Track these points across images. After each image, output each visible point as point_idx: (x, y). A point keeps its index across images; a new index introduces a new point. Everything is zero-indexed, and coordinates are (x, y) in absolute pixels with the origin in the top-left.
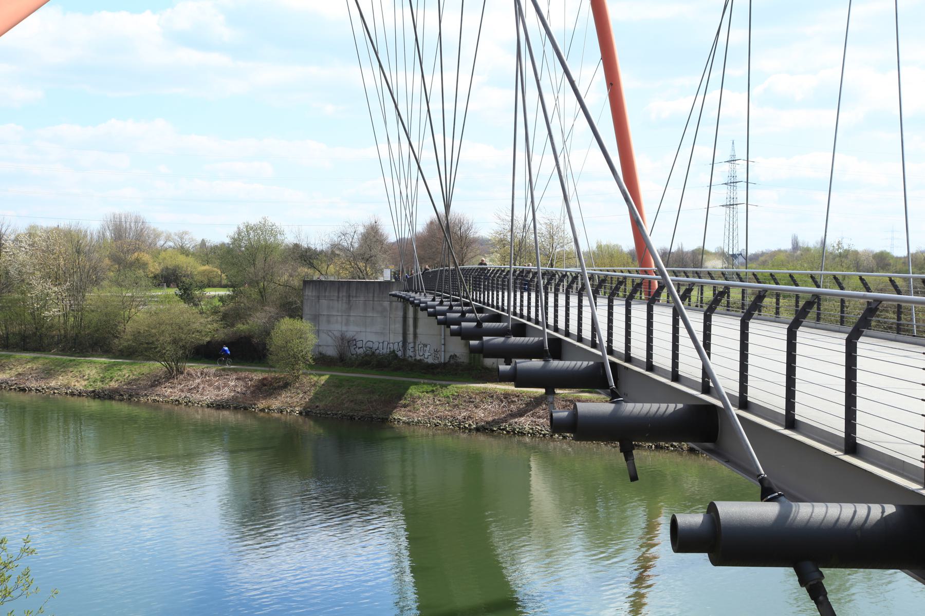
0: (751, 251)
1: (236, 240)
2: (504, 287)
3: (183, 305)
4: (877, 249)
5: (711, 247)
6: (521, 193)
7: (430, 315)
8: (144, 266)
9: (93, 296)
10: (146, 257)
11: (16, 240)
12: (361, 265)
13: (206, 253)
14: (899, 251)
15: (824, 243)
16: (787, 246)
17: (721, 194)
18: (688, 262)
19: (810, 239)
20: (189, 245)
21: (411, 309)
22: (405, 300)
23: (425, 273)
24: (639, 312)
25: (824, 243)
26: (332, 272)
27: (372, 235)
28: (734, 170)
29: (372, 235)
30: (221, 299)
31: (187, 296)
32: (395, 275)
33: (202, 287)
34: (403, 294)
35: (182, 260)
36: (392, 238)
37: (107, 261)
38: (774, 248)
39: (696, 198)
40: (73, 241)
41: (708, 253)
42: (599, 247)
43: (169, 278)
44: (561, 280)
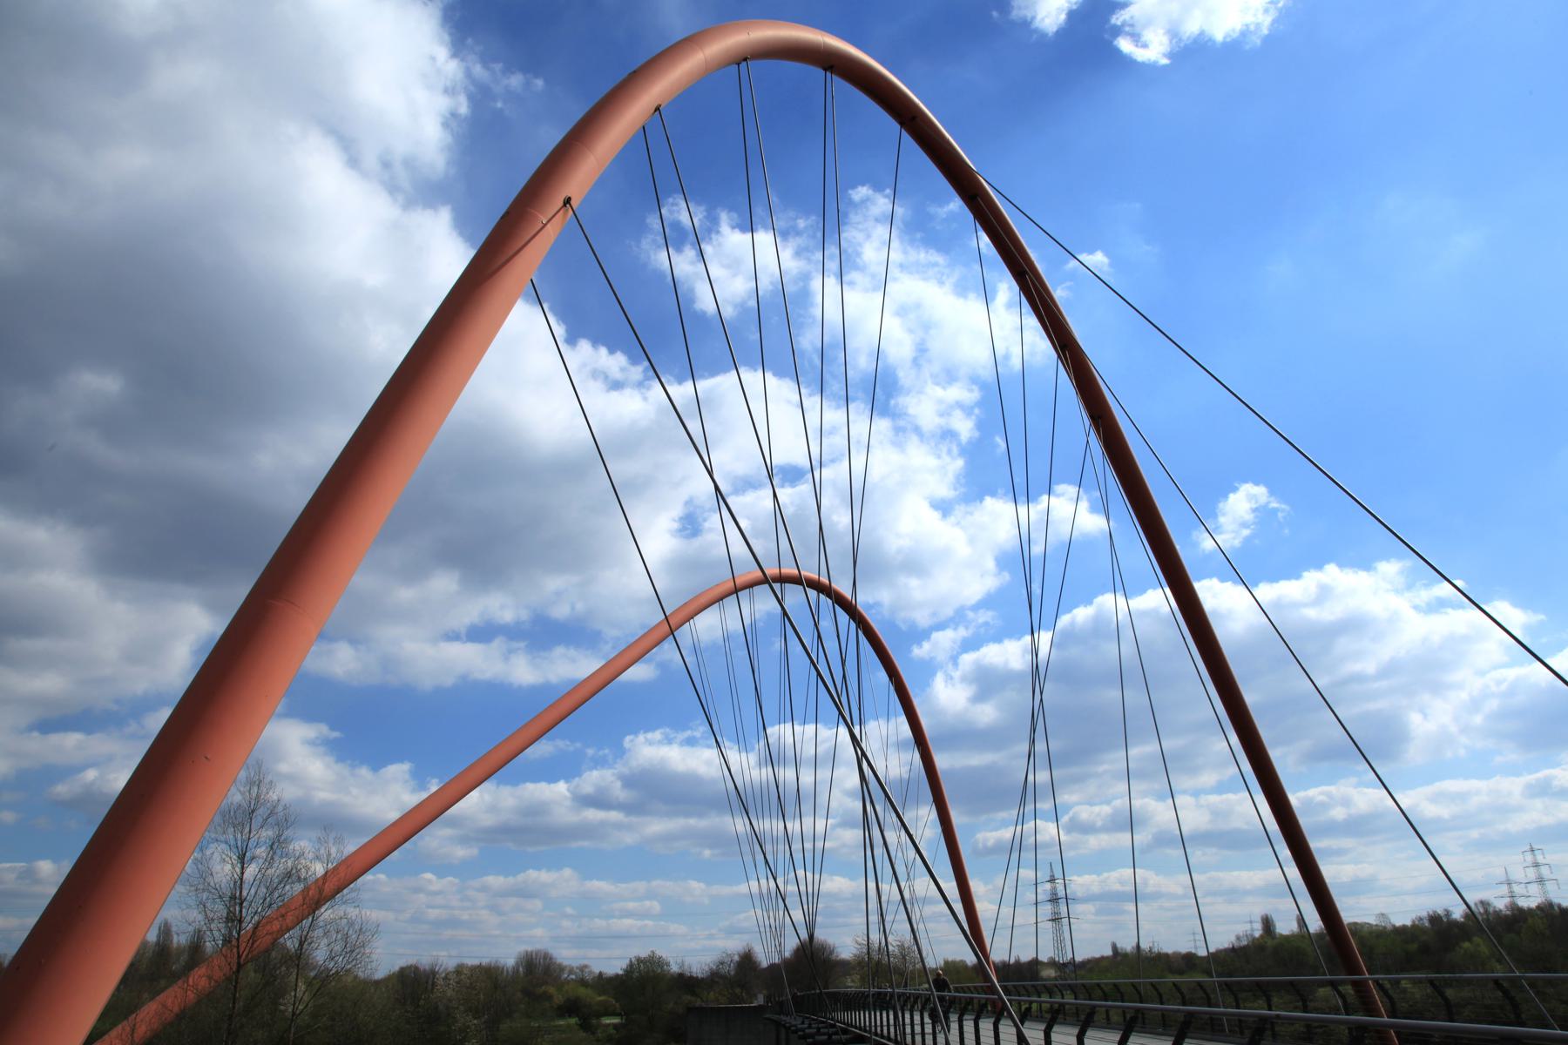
0: (1078, 959)
1: (630, 970)
2: (865, 1007)
3: (582, 1034)
4: (1184, 950)
5: (1043, 958)
6: (874, 918)
7: (800, 1038)
8: (549, 997)
9: (505, 1026)
10: (552, 990)
11: (445, 978)
12: (738, 990)
13: (604, 983)
14: (1202, 953)
15: (1138, 946)
16: (1108, 952)
17: (1046, 910)
18: (1022, 975)
19: (1127, 945)
20: (588, 977)
21: (783, 1032)
22: (778, 1024)
23: (794, 997)
24: (986, 1026)
25: (1138, 946)
26: (712, 999)
27: (747, 959)
28: (1054, 888)
29: (747, 959)
30: (615, 1026)
31: (585, 1026)
32: (768, 998)
33: (599, 1015)
34: (775, 1017)
35: (582, 991)
36: (764, 964)
37: (519, 995)
38: (1097, 955)
39: (1025, 916)
40: (489, 976)
41: (1042, 963)
42: (946, 963)
43: (572, 1007)
44: (915, 1002)
